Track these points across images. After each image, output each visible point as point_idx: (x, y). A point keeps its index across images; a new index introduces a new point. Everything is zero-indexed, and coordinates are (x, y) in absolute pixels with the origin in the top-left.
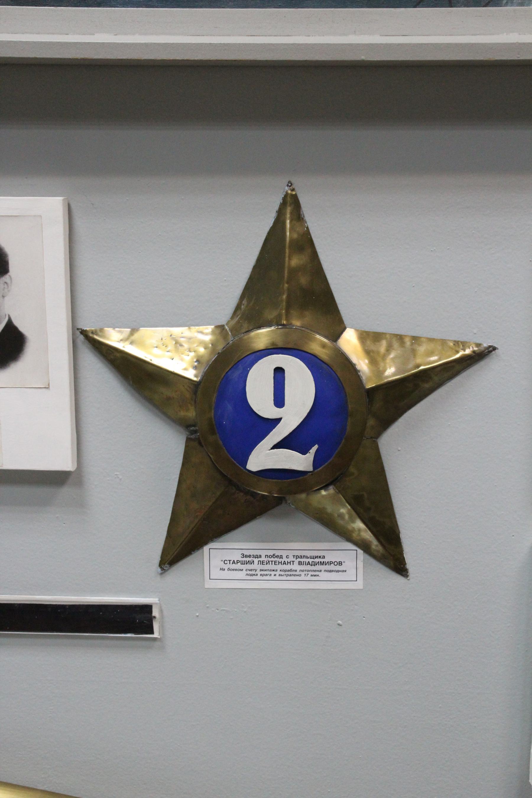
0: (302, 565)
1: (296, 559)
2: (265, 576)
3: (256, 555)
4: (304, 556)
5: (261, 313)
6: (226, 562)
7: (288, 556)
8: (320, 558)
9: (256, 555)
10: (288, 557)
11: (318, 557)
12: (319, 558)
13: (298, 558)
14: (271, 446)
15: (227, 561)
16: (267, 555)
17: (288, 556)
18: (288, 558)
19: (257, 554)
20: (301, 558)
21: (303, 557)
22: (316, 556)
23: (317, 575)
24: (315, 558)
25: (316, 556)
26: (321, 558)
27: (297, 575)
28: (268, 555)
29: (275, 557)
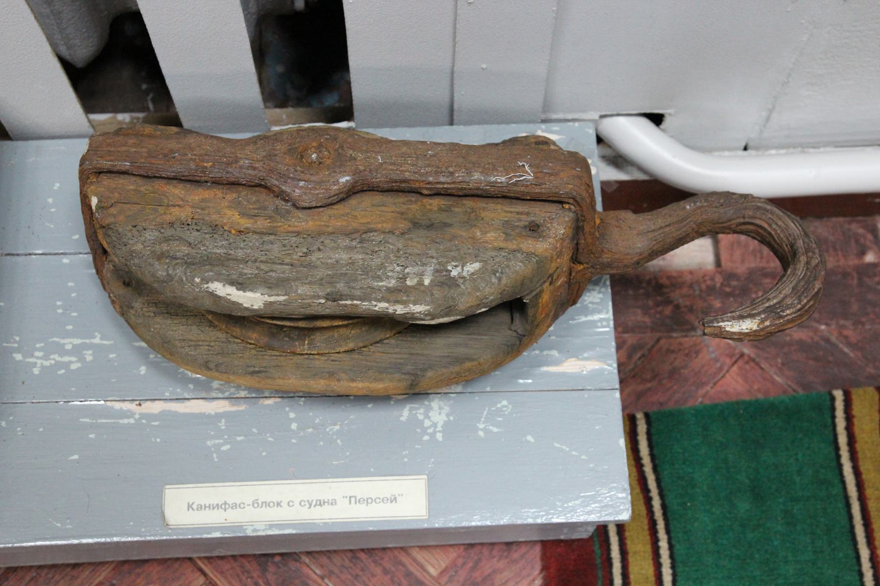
0: (259, 508)
1: (367, 505)
2: (230, 509)
3: (317, 500)
4: (262, 503)
5: (395, 203)
6: (303, 503)
7: (293, 502)
8: (190, 509)
9: (317, 500)
10: (291, 504)
11: (211, 507)
12: (277, 506)
13: (371, 503)
14: (648, 111)
15: (305, 502)
16: (353, 497)
17: (293, 502)
18: (293, 505)
19: (319, 498)
20: (234, 507)
21: (260, 505)
22: (394, 501)
23: (205, 507)
24: (322, 503)
25: (394, 501)
26: (193, 509)
27: (205, 507)
28: (355, 497)
29: (240, 505)
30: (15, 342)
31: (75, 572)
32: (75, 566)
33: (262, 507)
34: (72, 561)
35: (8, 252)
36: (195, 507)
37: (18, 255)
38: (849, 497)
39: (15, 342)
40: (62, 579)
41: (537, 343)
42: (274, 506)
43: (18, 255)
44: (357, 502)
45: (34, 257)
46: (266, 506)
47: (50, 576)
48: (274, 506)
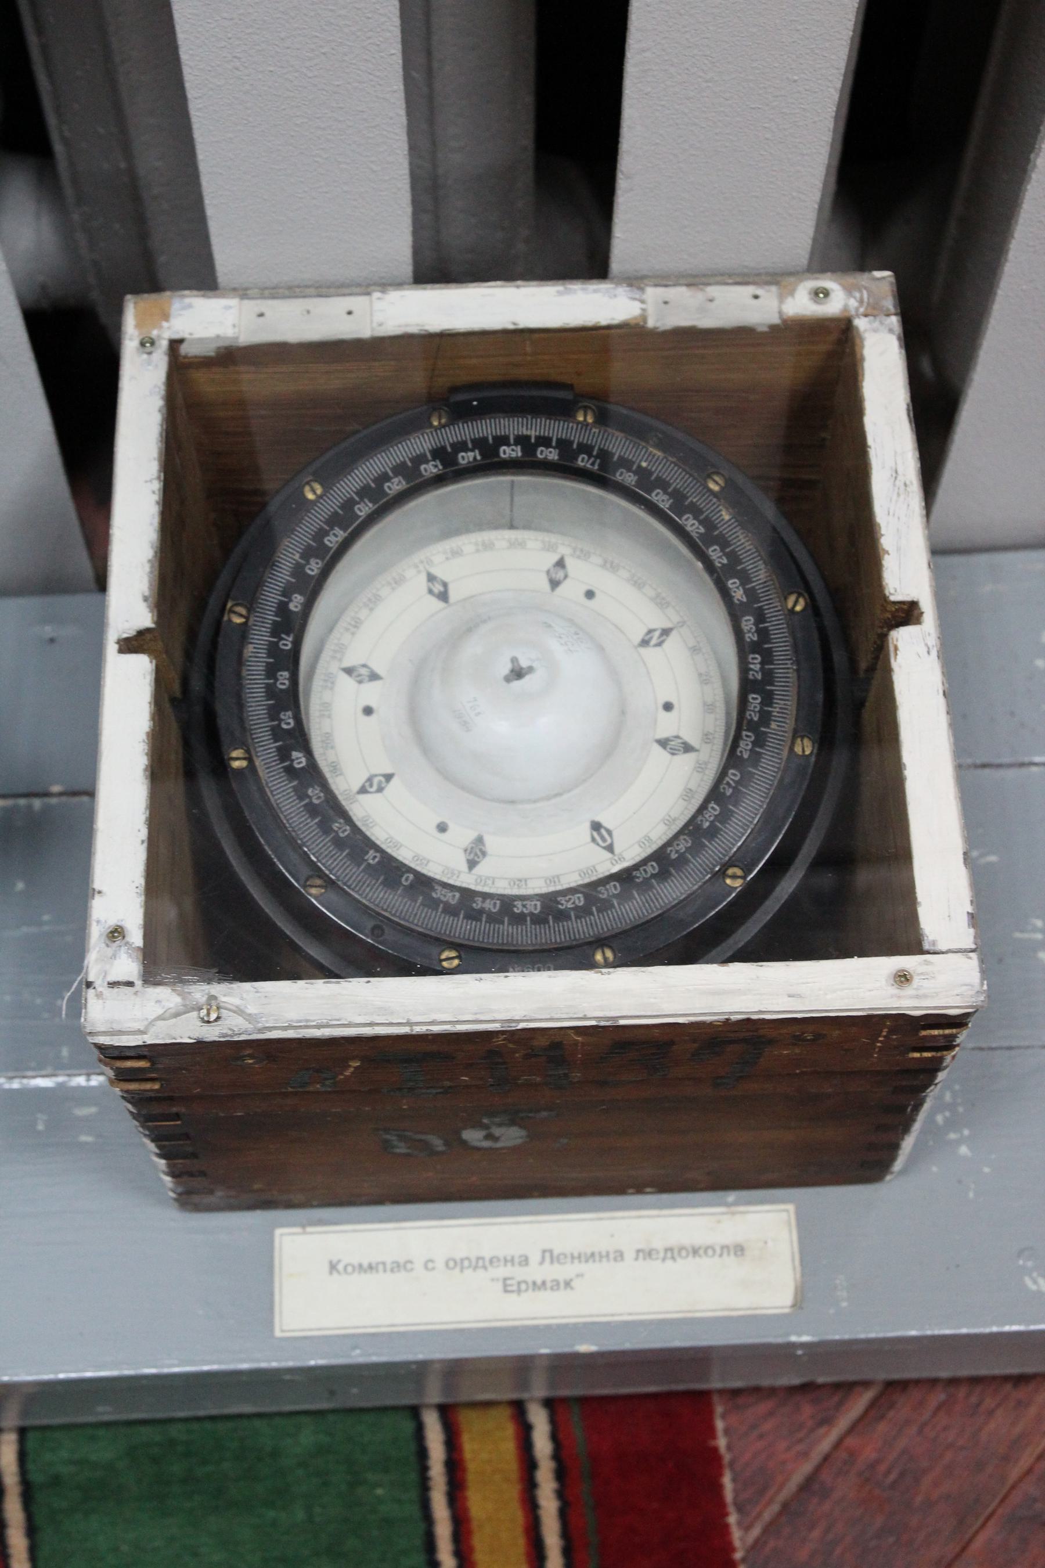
10: (430, 1265)
30: (1035, 930)
31: (1021, 1393)
32: (1020, 1380)
33: (721, 1255)
34: (1015, 1370)
35: (984, 760)
36: (340, 1267)
37: (999, 766)
38: (147, 754)
39: (1035, 930)
40: (999, 1405)
41: (644, 318)
42: (354, 1270)
43: (999, 766)
44: (555, 1260)
45: (1034, 769)
46: (552, 1262)
47: (974, 1399)
48: (354, 1270)
